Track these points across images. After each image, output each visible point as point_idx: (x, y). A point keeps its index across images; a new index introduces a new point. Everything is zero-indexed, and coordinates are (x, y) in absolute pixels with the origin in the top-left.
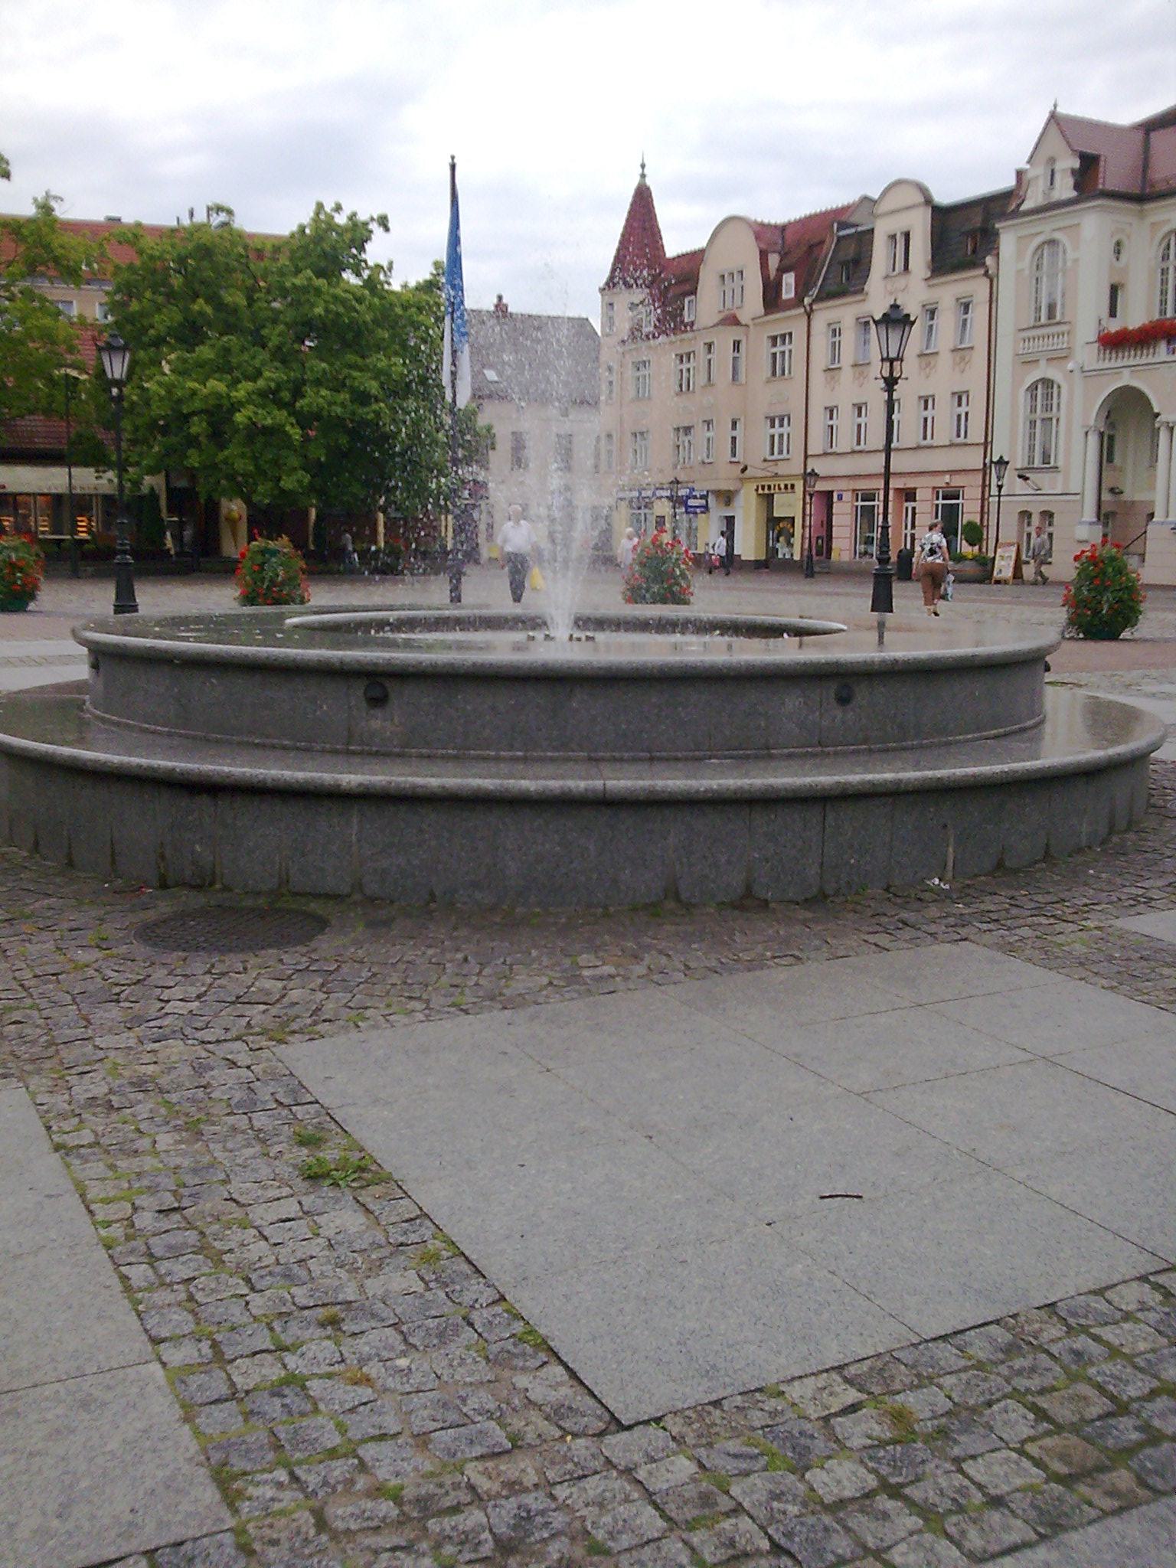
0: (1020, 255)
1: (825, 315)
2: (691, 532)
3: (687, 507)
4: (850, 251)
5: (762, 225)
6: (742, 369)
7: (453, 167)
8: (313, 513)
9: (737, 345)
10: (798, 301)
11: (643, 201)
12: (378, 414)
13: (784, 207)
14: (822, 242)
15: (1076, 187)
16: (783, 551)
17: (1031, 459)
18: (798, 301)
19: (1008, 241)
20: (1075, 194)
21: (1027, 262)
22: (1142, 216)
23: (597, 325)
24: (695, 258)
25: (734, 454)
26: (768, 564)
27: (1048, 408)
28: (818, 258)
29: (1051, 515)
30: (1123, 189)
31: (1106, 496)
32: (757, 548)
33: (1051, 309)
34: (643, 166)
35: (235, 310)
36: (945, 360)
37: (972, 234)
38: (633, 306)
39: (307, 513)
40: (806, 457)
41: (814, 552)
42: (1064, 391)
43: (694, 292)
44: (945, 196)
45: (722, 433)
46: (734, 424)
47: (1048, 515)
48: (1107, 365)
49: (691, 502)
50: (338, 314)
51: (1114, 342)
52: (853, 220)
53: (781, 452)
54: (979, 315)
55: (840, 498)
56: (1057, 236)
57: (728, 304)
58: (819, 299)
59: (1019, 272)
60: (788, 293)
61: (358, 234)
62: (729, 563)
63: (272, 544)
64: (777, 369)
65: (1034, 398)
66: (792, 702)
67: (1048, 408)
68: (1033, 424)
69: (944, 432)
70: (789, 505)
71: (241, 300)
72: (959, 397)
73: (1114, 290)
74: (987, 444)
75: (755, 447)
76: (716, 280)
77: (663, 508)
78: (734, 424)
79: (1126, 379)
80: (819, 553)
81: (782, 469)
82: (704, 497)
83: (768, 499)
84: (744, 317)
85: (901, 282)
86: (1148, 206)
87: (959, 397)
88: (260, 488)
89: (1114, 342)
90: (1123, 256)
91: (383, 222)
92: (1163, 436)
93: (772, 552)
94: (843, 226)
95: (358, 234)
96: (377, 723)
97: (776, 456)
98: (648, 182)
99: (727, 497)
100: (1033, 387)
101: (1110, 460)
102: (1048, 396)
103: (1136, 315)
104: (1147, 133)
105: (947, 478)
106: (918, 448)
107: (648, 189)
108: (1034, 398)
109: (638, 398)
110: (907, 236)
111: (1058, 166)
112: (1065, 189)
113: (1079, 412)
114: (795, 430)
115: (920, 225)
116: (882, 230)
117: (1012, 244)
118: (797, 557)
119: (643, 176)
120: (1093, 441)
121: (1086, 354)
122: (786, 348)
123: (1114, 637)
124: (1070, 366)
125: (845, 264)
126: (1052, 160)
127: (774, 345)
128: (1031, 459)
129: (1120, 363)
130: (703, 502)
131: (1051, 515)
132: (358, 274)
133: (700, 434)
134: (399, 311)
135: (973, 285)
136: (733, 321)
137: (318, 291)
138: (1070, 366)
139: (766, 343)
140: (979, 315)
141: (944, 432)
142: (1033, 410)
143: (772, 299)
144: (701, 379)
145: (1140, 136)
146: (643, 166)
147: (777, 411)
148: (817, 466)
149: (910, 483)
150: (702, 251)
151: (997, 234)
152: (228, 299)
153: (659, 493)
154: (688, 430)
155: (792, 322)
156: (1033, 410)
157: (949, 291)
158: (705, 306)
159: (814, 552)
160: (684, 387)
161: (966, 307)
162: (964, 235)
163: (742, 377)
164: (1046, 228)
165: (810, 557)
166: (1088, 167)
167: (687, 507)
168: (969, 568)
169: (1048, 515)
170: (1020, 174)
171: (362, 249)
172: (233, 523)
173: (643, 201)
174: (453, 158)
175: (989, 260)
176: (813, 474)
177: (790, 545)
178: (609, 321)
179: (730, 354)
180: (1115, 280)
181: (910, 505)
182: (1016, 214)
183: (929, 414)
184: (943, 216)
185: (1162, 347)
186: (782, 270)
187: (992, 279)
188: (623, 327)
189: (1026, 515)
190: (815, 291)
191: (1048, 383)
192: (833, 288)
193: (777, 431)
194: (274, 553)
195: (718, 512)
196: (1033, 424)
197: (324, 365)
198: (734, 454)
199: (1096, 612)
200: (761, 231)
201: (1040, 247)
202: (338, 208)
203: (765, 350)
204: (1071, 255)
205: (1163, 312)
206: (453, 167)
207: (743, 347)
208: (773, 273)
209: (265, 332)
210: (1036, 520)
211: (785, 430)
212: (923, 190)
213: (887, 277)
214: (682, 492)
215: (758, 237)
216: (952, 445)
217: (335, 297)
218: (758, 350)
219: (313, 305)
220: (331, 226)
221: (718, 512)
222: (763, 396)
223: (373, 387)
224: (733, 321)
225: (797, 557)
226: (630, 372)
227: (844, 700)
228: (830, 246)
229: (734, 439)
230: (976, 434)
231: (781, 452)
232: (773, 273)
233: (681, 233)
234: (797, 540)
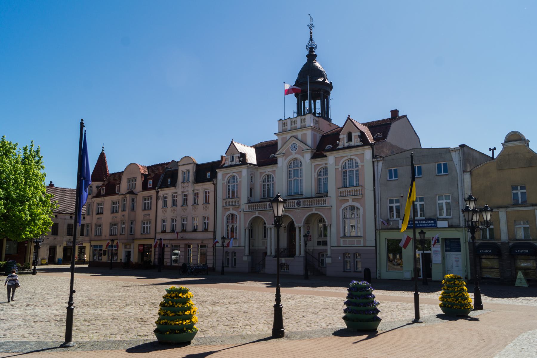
10: (153, 188)
19: (220, 174)
24: (119, 175)
29: (235, 253)
33: (233, 192)
34: (311, 26)
40: (156, 233)
42: (238, 217)
44: (199, 162)
55: (167, 246)
59: (223, 183)
73: (251, 190)
85: (186, 184)
100: (228, 216)
101: (252, 237)
102: (233, 219)
107: (104, 154)
111: (234, 156)
115: (192, 169)
116: (181, 169)
119: (103, 150)
120: (247, 231)
131: (235, 253)
135: (209, 186)
136: (131, 193)
143: (145, 187)
146: (103, 148)
149: (190, 242)
150: (122, 172)
155: (153, 193)
157: (201, 188)
158: (124, 186)
170: (222, 157)
174: (82, 120)
182: (222, 167)
183: (165, 224)
187: (215, 185)
191: (233, 215)
229: (131, 228)
230: (211, 228)
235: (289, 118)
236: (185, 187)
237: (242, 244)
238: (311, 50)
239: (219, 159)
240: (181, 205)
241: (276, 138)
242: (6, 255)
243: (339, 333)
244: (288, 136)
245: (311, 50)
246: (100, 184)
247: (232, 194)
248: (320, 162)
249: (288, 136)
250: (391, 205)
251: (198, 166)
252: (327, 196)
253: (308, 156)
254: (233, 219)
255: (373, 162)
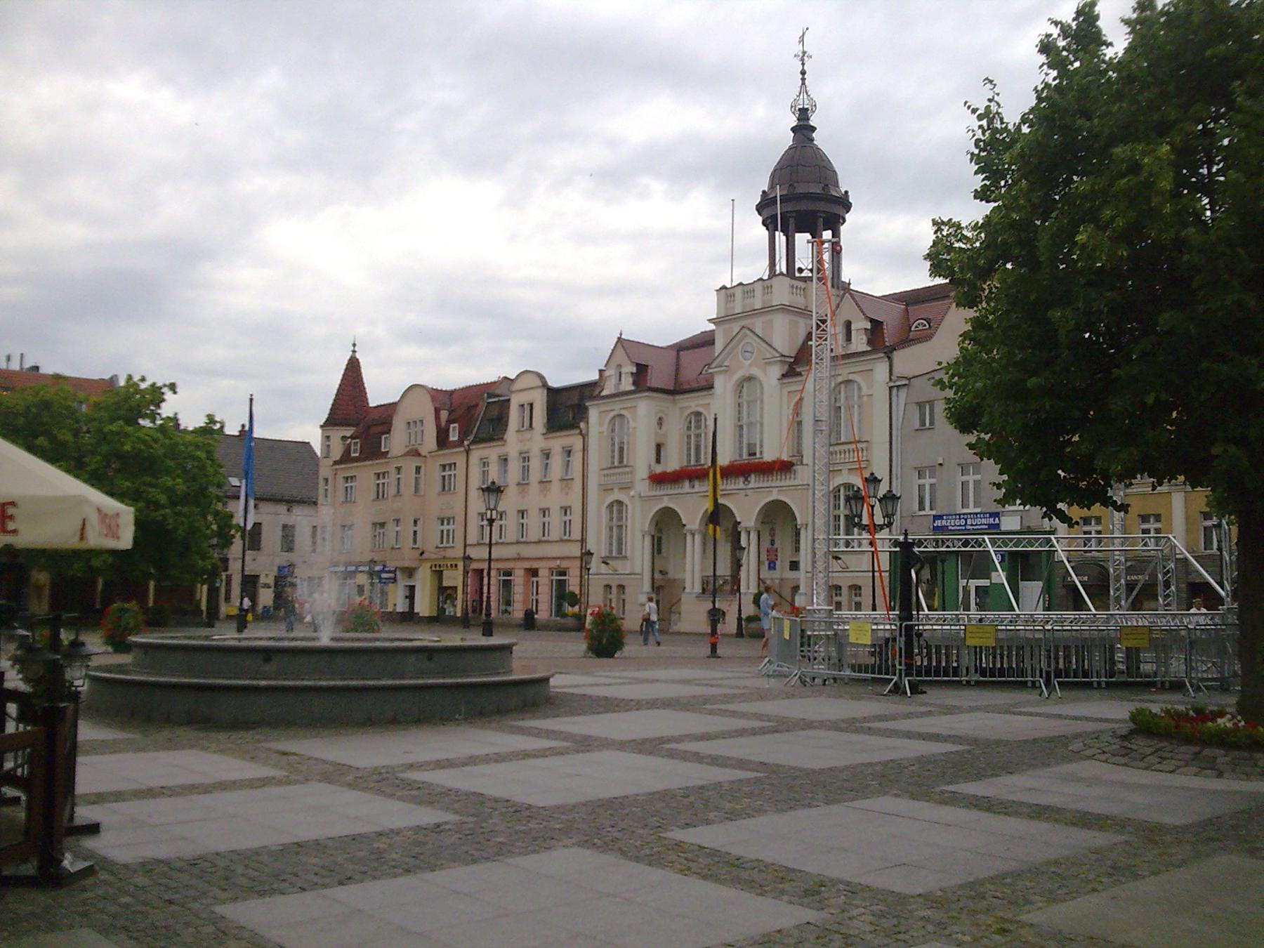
0: (601, 425)
1: (477, 453)
2: (384, 593)
3: (380, 578)
4: (494, 413)
5: (436, 390)
6: (422, 486)
7: (251, 400)
8: (100, 582)
9: (418, 469)
10: (460, 443)
11: (353, 367)
12: (164, 516)
13: (456, 375)
14: (477, 405)
15: (634, 383)
16: (449, 610)
17: (611, 551)
18: (460, 443)
20: (633, 388)
21: (605, 428)
22: (674, 402)
23: (318, 449)
24: (390, 408)
25: (415, 541)
26: (439, 619)
27: (620, 519)
28: (473, 415)
30: (663, 387)
31: (657, 576)
32: (428, 605)
34: (354, 345)
35: (64, 444)
36: (556, 487)
37: (572, 407)
38: (344, 438)
39: (95, 583)
40: (465, 546)
41: (470, 610)
43: (388, 432)
44: (555, 383)
45: (407, 529)
46: (415, 522)
47: (621, 587)
48: (654, 493)
49: (384, 575)
50: (141, 450)
51: (659, 479)
52: (498, 392)
53: (448, 542)
54: (577, 458)
56: (623, 412)
57: (413, 442)
58: (473, 442)
59: (601, 433)
60: (454, 437)
61: (156, 395)
62: (409, 617)
63: (126, 605)
64: (446, 485)
65: (611, 512)
66: (412, 659)
67: (620, 519)
68: (611, 529)
69: (555, 533)
70: (454, 578)
71: (69, 437)
72: (565, 510)
73: (659, 447)
74: (583, 541)
75: (431, 538)
76: (404, 426)
77: (362, 579)
78: (415, 522)
79: (666, 503)
80: (474, 611)
81: (449, 553)
82: (394, 572)
83: (439, 574)
84: (424, 451)
85: (527, 435)
86: (677, 397)
87: (565, 510)
88: (76, 566)
89: (659, 479)
90: (664, 428)
91: (173, 387)
92: (689, 538)
93: (441, 610)
94: (490, 396)
95: (156, 395)
96: (266, 668)
97: (445, 544)
98: (358, 355)
99: (410, 572)
100: (611, 506)
101: (659, 552)
102: (620, 512)
103: (673, 463)
104: (678, 351)
105: (558, 562)
106: (539, 542)
108: (611, 512)
109: (346, 501)
110: (531, 405)
111: (623, 370)
112: (627, 384)
113: (639, 522)
114: (458, 527)
116: (515, 401)
117: (596, 416)
118: (459, 615)
119: (354, 351)
120: (648, 540)
121: (642, 486)
122: (453, 473)
123: (612, 656)
124: (632, 493)
125: (491, 421)
126: (620, 366)
127: (444, 470)
128: (611, 551)
129: (662, 493)
130: (392, 575)
132: (153, 421)
133: (391, 529)
134: (182, 448)
135: (574, 441)
136: (415, 453)
137: (127, 435)
138: (632, 493)
139: (438, 468)
140: (577, 458)
141: (555, 533)
142: (611, 519)
143: (442, 440)
144: (392, 491)
145: (674, 353)
146: (354, 345)
147: (447, 514)
148: (472, 553)
149: (535, 565)
151: (587, 408)
152: (61, 437)
153: (361, 568)
154: (382, 525)
156: (611, 519)
157: (557, 443)
158: (396, 442)
159: (470, 610)
160: (380, 496)
161: (569, 453)
162: (567, 407)
163: (422, 493)
164: (617, 407)
165: (467, 614)
166: (641, 372)
167: (380, 578)
168: (570, 621)
169: (621, 587)
170: (601, 371)
171: (158, 407)
172: (39, 588)
173: (353, 367)
175: (582, 425)
176: (469, 558)
177: (455, 606)
178: (327, 448)
179: (414, 475)
180: (659, 441)
181: (535, 579)
182: (599, 397)
183: (546, 519)
184: (554, 394)
185: (687, 483)
186: (449, 422)
187: (584, 436)
188: (337, 453)
189: (608, 587)
190: (471, 438)
191: (620, 503)
192: (483, 436)
193: (445, 527)
194: (127, 610)
195: (403, 582)
196: (611, 529)
197: (128, 484)
198: (415, 541)
199: (600, 643)
200: (436, 394)
201: (614, 418)
202: (143, 379)
203: (437, 474)
204: (632, 424)
205: (689, 461)
206: (251, 400)
207: (422, 470)
208: (443, 424)
209: (87, 460)
210: (614, 590)
211: (451, 527)
212: (541, 377)
213: (518, 431)
214: (377, 568)
215: (434, 399)
216: (562, 541)
217: (138, 438)
218: (433, 473)
219: (123, 444)
220: (138, 391)
221: (403, 582)
222: (435, 504)
223: (163, 499)
224: (415, 453)
225: (459, 615)
226: (341, 484)
227: (430, 659)
228: (482, 407)
230: (576, 535)
231: (448, 542)
232: (443, 424)
233: (381, 388)
234: (459, 603)
235: (741, 284)
236: (525, 437)
237: (638, 570)
238: (803, 114)
239: (596, 377)
240: (516, 481)
241: (712, 327)
242: (238, 498)
243: (13, 504)
244: (736, 327)
245: (803, 114)
246: (348, 432)
247: (620, 455)
248: (794, 385)
249: (736, 327)
250: (965, 478)
251: (553, 393)
252: (802, 464)
253: (776, 371)
254: (620, 512)
255: (891, 388)
